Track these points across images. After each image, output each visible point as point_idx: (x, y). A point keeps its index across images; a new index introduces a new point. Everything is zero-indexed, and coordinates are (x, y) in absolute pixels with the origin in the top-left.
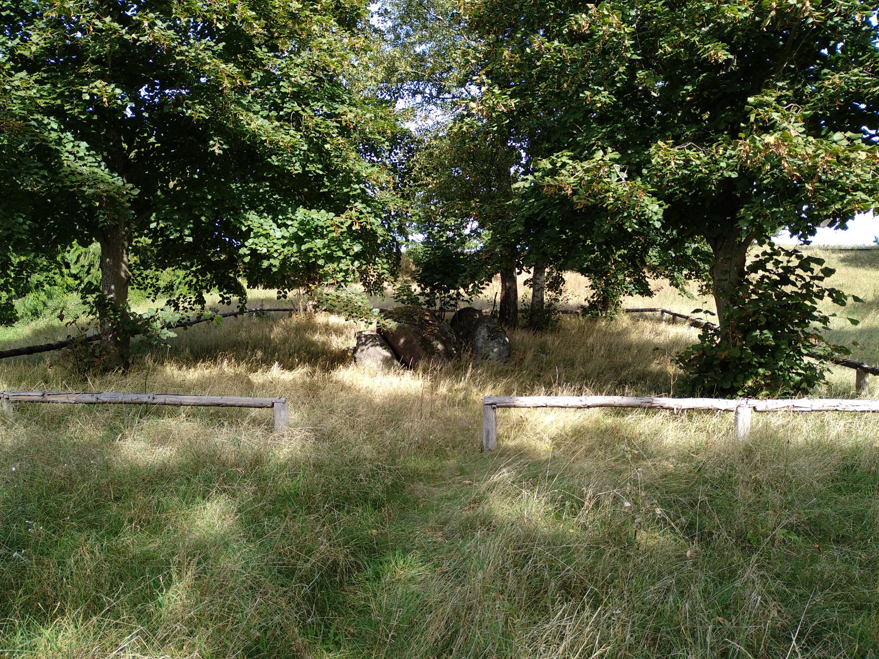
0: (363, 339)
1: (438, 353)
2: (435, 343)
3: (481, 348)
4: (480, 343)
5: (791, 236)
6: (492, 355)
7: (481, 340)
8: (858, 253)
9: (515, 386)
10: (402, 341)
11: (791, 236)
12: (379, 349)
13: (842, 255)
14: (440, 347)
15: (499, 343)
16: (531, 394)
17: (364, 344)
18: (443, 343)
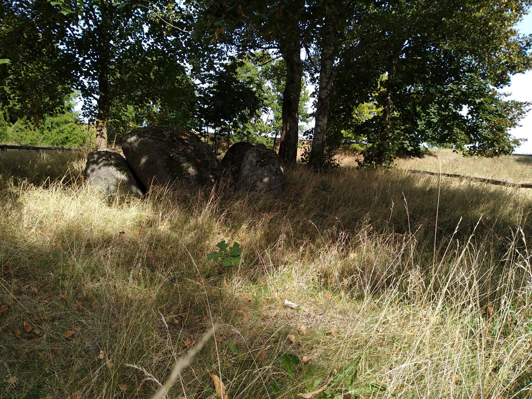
0: (96, 156)
1: (188, 179)
2: (185, 165)
3: (247, 176)
4: (246, 170)
5: (515, 128)
6: (260, 185)
7: (248, 167)
8: (528, 157)
9: (286, 228)
10: (143, 160)
11: (515, 128)
12: (112, 169)
13: (517, 157)
14: (191, 170)
15: (270, 171)
16: (46, 187)
17: (96, 162)
18: (197, 166)
